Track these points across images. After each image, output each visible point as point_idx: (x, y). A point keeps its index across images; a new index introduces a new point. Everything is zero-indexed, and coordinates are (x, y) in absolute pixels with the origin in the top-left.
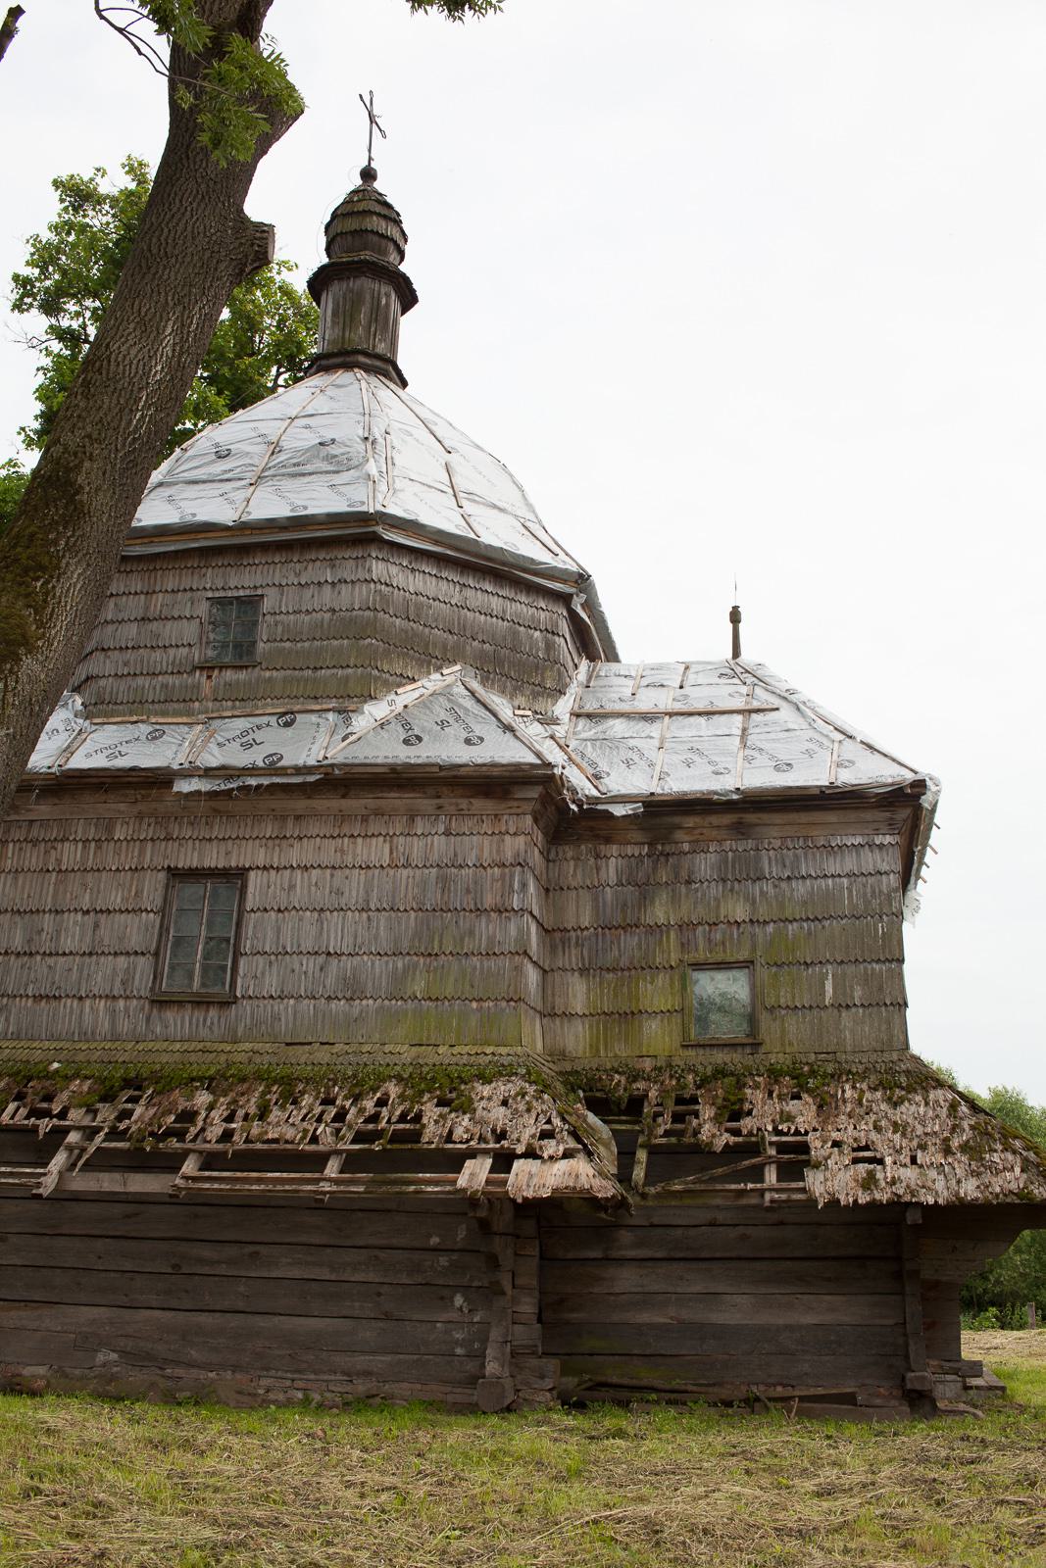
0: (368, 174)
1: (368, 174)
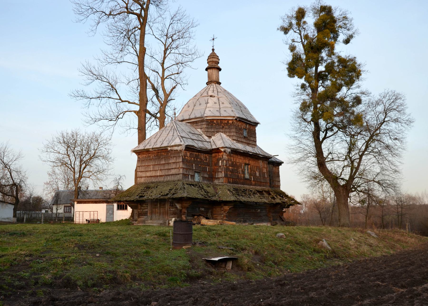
0: (213, 50)
1: (213, 50)
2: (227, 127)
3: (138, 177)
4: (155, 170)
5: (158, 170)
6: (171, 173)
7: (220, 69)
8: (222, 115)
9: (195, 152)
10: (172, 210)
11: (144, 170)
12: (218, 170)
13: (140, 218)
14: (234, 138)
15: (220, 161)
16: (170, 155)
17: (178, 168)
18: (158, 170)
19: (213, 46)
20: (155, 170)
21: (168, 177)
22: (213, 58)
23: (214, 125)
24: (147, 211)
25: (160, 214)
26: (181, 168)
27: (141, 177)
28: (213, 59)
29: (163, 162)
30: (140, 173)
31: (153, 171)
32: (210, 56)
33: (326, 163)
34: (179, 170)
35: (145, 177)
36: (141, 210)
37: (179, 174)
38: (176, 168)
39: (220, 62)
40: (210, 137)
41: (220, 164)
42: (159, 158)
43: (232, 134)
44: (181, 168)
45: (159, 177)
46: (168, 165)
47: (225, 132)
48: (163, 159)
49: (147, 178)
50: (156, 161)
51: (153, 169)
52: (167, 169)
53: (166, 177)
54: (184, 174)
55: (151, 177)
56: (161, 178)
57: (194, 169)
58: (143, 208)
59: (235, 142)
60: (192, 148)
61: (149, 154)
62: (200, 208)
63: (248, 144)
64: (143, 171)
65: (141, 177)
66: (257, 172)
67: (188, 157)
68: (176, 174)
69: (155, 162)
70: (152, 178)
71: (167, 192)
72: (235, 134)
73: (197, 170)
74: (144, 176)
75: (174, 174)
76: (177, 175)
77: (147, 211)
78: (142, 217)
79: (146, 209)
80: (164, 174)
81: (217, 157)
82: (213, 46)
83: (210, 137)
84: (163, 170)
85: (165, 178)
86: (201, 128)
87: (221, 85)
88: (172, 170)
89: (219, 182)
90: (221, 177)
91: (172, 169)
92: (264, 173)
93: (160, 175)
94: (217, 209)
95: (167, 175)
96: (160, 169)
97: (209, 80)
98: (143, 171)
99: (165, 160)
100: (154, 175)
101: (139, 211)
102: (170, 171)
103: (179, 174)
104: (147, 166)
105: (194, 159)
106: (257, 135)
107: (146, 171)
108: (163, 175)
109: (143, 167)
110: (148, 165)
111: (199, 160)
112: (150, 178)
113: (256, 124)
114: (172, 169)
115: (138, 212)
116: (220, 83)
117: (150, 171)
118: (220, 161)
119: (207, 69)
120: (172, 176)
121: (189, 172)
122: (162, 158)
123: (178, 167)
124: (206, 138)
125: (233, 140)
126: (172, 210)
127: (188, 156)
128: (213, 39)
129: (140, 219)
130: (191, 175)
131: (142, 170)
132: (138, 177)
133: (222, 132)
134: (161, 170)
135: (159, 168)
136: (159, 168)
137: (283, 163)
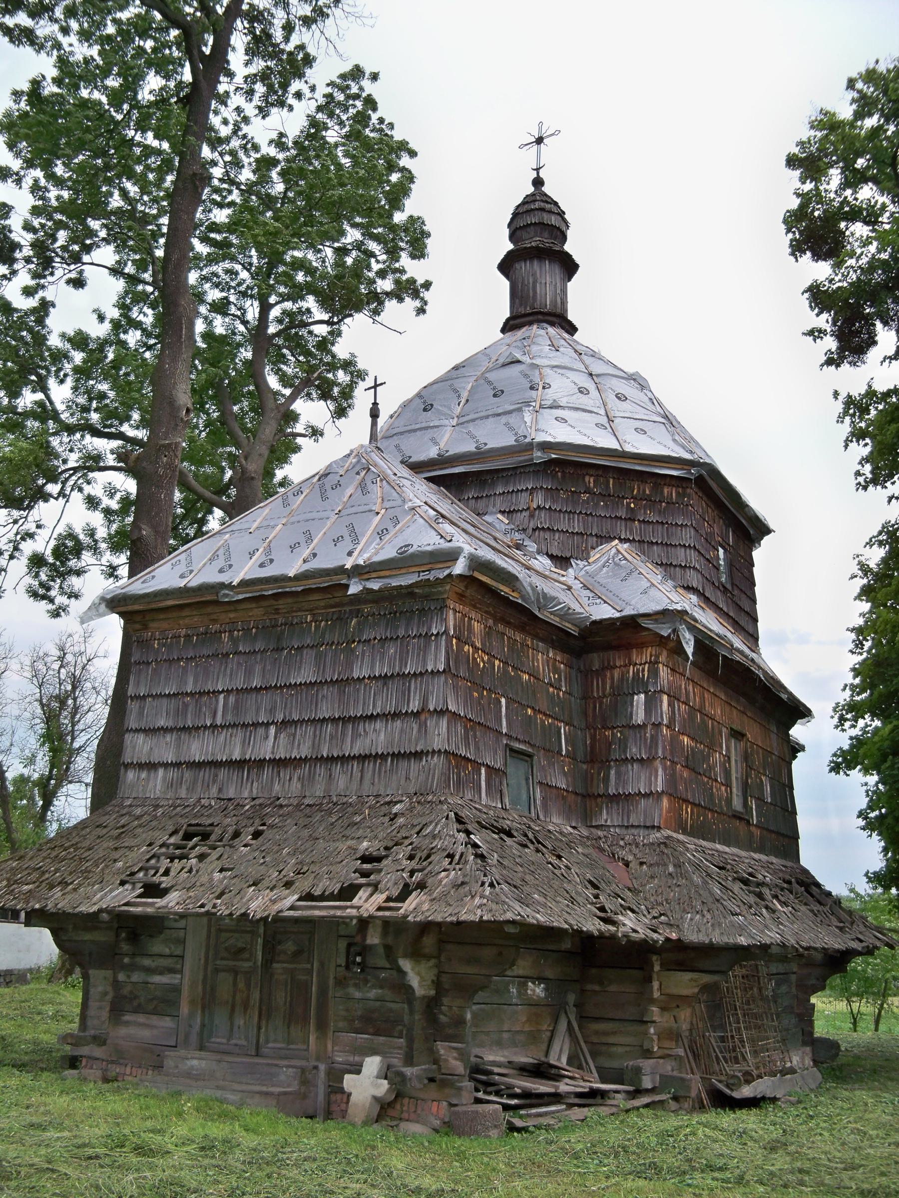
0: (538, 182)
1: (538, 182)
2: (653, 518)
3: (127, 766)
4: (245, 726)
5: (267, 725)
6: (358, 749)
7: (569, 267)
8: (628, 448)
9: (508, 624)
10: (357, 995)
11: (170, 724)
12: (624, 747)
13: (127, 1023)
14: (695, 580)
15: (640, 699)
16: (360, 628)
17: (417, 715)
18: (267, 725)
19: (537, 170)
20: (245, 726)
21: (337, 769)
22: (542, 210)
23: (585, 497)
24: (176, 989)
25: (266, 1012)
26: (440, 713)
27: (151, 766)
28: (545, 215)
29: (306, 674)
30: (141, 737)
31: (234, 726)
32: (524, 203)
33: (131, 775)
34: (423, 727)
35: (177, 765)
36: (136, 977)
37: (418, 755)
38: (396, 715)
39: (570, 233)
40: (562, 561)
41: (639, 716)
42: (279, 649)
43: (681, 557)
44: (440, 713)
45: (267, 772)
46: (190, 733)
47: (642, 545)
48: (309, 655)
49: (188, 775)
50: (258, 668)
51: (230, 718)
52: (334, 720)
53: (321, 771)
54: (455, 755)
55: (215, 764)
56: (285, 774)
57: (504, 731)
58: (147, 962)
59: (694, 598)
60: (504, 590)
61: (214, 621)
62: (525, 985)
63: (738, 627)
64: (165, 730)
65: (151, 766)
66: (763, 778)
67: (476, 649)
68: (398, 756)
69: (249, 673)
70: (222, 773)
71: (347, 872)
72: (693, 558)
73: (517, 739)
74: (170, 758)
75: (383, 757)
76: (403, 764)
77: (176, 989)
78: (141, 1018)
79: (171, 971)
80: (305, 751)
81: (617, 673)
82: (537, 170)
83: (562, 561)
84: (302, 722)
85: (311, 777)
86: (508, 513)
87: (576, 336)
88: (370, 727)
89: (633, 820)
90: (647, 795)
91: (371, 718)
92: (784, 784)
93: (281, 754)
94: (613, 988)
95: (331, 759)
96: (280, 717)
97: (522, 310)
98: (165, 730)
99: (319, 657)
100: (236, 756)
101: (121, 977)
102: (356, 736)
103: (418, 755)
104: (192, 694)
105: (506, 672)
106: (759, 591)
107: (184, 729)
108: (305, 760)
109: (165, 701)
110: (201, 694)
111: (526, 677)
112: (205, 774)
113: (764, 530)
114: (371, 718)
115: (116, 984)
116: (571, 329)
117: (214, 727)
118: (640, 699)
119: (506, 266)
120: (369, 767)
121: (477, 748)
122: (300, 649)
123: (414, 705)
124: (543, 563)
125: (689, 588)
126: (357, 995)
127: (479, 645)
128: (539, 141)
129: (123, 1031)
130: (488, 766)
131: (161, 723)
132: (127, 766)
133: (626, 540)
134: (285, 724)
135: (272, 711)
136: (272, 711)
137: (802, 748)
